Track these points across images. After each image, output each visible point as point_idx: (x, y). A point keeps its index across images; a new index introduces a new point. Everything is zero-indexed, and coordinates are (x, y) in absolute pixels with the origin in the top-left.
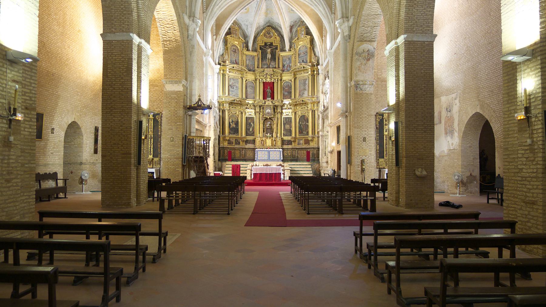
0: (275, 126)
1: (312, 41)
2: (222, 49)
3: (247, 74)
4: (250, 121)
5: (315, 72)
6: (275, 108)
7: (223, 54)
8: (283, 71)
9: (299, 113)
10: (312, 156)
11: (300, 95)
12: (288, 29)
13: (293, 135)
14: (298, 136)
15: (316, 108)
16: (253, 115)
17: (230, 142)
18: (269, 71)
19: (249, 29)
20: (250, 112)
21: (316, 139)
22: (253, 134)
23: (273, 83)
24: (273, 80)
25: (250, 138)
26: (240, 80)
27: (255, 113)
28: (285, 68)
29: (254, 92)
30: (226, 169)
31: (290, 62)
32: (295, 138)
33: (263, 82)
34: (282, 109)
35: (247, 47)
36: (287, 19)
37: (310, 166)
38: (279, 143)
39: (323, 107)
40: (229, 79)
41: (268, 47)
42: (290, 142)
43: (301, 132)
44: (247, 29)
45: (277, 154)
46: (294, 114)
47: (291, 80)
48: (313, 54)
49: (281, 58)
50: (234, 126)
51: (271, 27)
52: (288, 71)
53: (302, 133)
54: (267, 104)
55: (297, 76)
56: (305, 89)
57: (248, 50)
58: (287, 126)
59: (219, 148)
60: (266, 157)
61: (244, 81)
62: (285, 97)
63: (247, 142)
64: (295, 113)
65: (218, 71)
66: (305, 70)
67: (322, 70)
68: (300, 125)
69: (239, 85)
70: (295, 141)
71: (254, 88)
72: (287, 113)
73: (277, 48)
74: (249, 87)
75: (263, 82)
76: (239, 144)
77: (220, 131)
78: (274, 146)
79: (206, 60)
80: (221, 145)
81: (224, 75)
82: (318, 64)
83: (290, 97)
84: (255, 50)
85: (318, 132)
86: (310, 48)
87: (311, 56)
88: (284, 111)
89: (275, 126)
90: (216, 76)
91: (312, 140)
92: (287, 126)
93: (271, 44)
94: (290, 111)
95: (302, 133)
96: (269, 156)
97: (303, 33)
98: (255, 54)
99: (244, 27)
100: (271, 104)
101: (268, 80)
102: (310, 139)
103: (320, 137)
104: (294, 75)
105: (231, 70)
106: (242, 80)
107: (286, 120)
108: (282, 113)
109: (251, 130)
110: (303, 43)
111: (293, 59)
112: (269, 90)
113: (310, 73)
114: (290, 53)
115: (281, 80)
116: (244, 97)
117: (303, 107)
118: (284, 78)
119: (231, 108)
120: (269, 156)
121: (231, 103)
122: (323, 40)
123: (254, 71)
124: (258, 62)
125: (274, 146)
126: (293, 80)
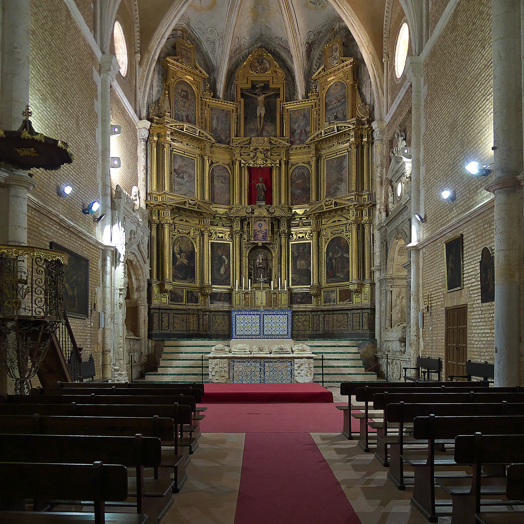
0: (275, 262)
1: (358, 65)
2: (155, 89)
3: (214, 149)
5: (365, 140)
6: (275, 222)
7: (158, 101)
8: (292, 143)
9: (328, 235)
10: (363, 328)
11: (329, 194)
12: (303, 49)
13: (314, 280)
14: (324, 283)
15: (366, 218)
16: (227, 240)
17: (175, 297)
18: (260, 143)
19: (218, 50)
20: (222, 234)
21: (367, 289)
22: (226, 281)
23: (270, 169)
24: (269, 161)
25: (218, 289)
26: (197, 162)
27: (231, 236)
28: (297, 137)
29: (230, 189)
30: (164, 356)
31: (308, 124)
32: (319, 287)
33: (249, 168)
34: (289, 227)
35: (213, 89)
36: (301, 23)
37: (355, 350)
38: (284, 299)
39: (384, 214)
40: (173, 158)
41: (258, 90)
42: (306, 298)
43: (331, 275)
44: (214, 51)
45: (279, 322)
46: (315, 234)
47: (309, 163)
48: (359, 100)
49: (286, 116)
50: (185, 261)
51: (266, 50)
52: (302, 142)
53: (334, 276)
54: (256, 214)
55: (323, 152)
56: (341, 180)
57: (215, 96)
58: (301, 263)
59: (149, 309)
60: (255, 330)
61: (207, 164)
62: (296, 200)
63: (214, 297)
64: (319, 235)
65: (145, 134)
66: (342, 135)
67: (382, 132)
68: (329, 260)
69: (197, 172)
70: (317, 296)
71: (229, 181)
72: (301, 233)
73: (278, 95)
74: (220, 177)
75: (249, 168)
76: (197, 302)
77: (151, 272)
78: (272, 304)
79: (104, 82)
80: (155, 302)
81: (160, 146)
82: (370, 120)
83: (307, 200)
84: (229, 97)
85: (372, 273)
86: (353, 86)
87: (354, 106)
88: (293, 230)
89: (275, 262)
90: (141, 147)
91: (358, 292)
92: (301, 263)
93: (266, 87)
94: (307, 229)
95: (334, 276)
97: (337, 54)
98: (230, 106)
99: (206, 47)
100: (265, 214)
101: (260, 162)
102: (352, 287)
103: (377, 285)
104: (317, 150)
105: (177, 133)
106: (203, 160)
107: (298, 250)
108: (289, 235)
109: (222, 271)
110: (336, 75)
111: (314, 115)
112: (261, 185)
113: (352, 139)
114: (307, 104)
115: (287, 163)
116: (207, 197)
117: (336, 219)
118: (294, 159)
119: (177, 221)
121: (178, 210)
122: (382, 64)
123: (229, 143)
124: (238, 123)
125: (272, 304)
126: (313, 163)
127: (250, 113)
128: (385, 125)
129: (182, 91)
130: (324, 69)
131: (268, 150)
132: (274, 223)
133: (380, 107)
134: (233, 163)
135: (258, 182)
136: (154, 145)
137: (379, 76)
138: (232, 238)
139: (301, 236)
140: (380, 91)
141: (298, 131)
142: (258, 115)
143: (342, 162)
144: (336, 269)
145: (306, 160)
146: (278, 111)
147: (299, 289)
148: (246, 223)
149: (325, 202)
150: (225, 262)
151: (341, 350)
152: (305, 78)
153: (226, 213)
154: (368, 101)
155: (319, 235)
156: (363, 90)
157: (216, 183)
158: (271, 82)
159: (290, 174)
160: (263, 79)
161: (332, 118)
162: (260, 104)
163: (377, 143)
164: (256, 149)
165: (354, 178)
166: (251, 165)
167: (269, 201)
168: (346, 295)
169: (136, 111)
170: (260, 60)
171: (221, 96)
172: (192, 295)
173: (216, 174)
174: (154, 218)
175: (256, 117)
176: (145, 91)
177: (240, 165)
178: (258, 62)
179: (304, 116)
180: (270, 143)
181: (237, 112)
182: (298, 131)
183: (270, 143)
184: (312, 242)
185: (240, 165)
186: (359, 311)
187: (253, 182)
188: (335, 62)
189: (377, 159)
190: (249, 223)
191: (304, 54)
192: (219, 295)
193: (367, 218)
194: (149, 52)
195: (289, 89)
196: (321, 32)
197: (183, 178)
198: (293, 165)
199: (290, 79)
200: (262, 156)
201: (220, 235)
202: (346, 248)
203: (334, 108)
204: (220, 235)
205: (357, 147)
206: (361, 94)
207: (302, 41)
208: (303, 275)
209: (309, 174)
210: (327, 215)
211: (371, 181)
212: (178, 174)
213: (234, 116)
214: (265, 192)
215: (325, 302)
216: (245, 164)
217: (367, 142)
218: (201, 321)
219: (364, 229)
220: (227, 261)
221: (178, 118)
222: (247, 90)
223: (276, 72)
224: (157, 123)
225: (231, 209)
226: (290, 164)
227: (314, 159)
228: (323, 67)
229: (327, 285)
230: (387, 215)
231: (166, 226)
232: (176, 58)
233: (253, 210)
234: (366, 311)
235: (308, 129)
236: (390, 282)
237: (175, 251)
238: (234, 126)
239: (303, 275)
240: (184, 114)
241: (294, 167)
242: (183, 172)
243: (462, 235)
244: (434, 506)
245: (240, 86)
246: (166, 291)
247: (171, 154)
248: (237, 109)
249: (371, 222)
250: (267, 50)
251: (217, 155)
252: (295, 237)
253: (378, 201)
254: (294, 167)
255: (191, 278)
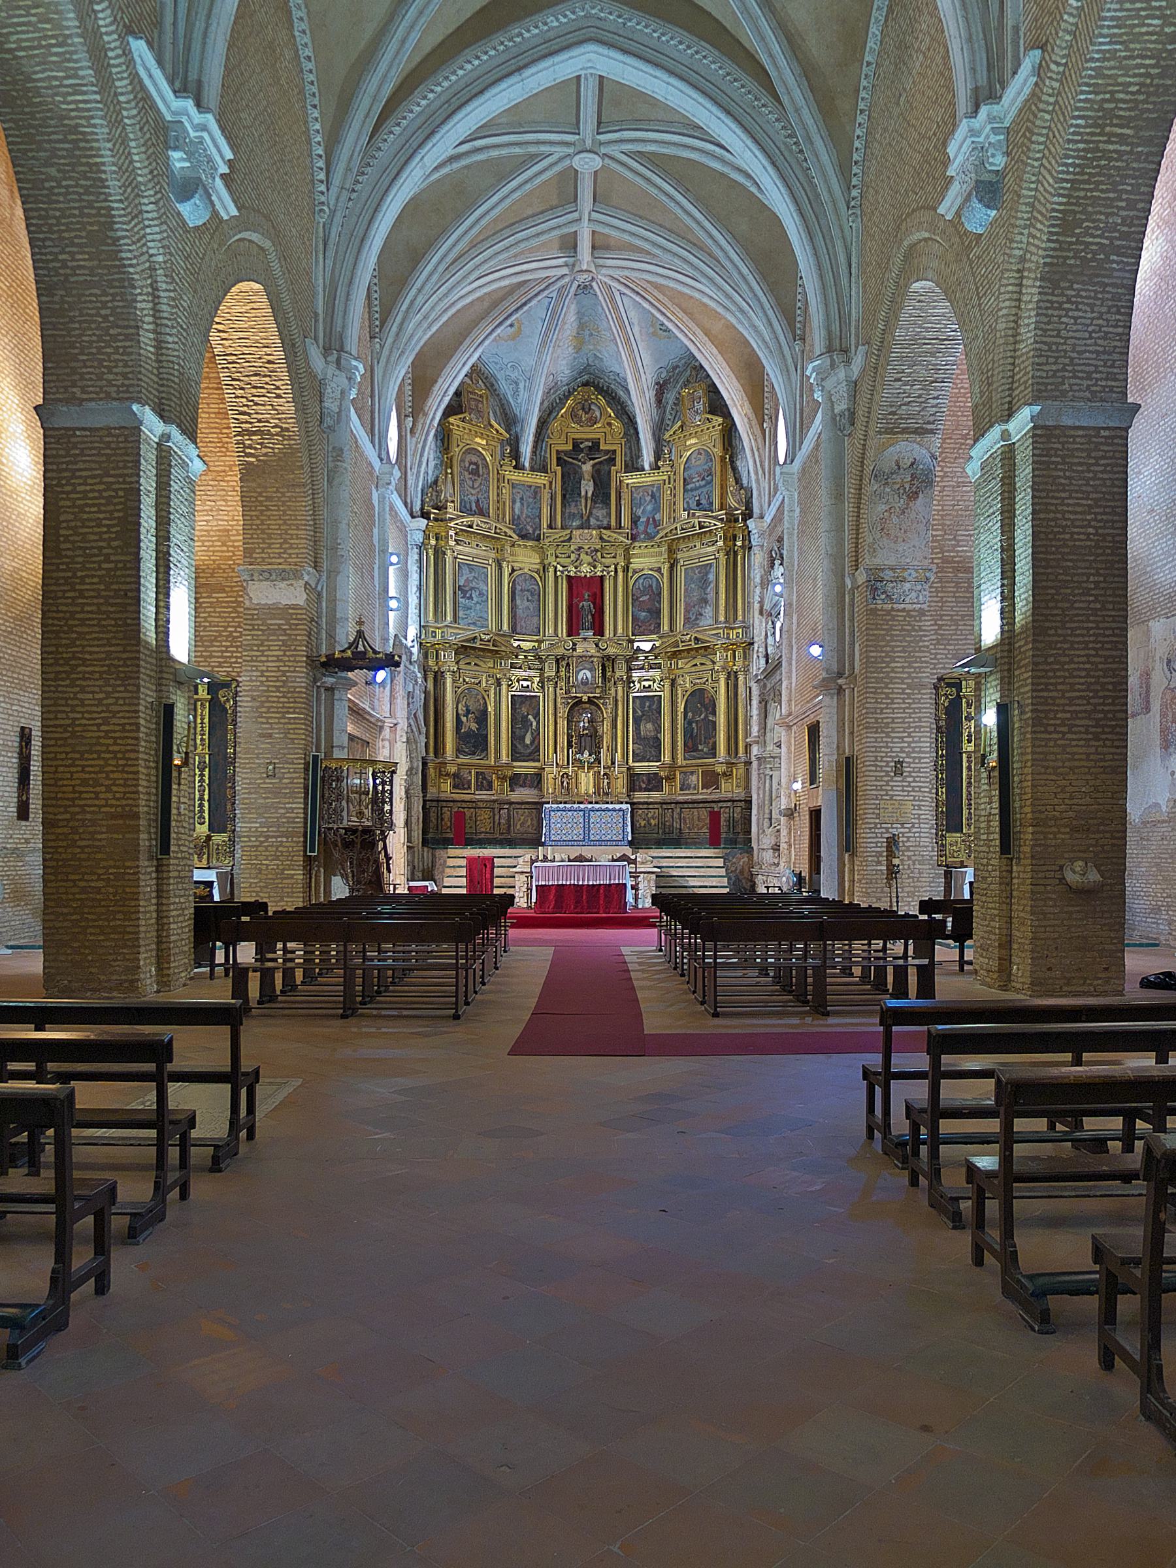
0: (607, 726)
1: (729, 433)
4: (524, 710)
6: (608, 663)
7: (436, 482)
8: (634, 538)
9: (686, 684)
10: (729, 829)
12: (650, 394)
13: (666, 757)
14: (680, 761)
15: (739, 663)
18: (587, 538)
19: (523, 395)
20: (524, 680)
22: (533, 754)
25: (525, 767)
26: (492, 570)
28: (641, 528)
29: (539, 610)
30: (448, 871)
31: (657, 509)
32: (673, 767)
34: (630, 669)
35: (516, 455)
39: (763, 661)
42: (654, 782)
43: (691, 747)
44: (516, 393)
46: (667, 684)
47: (659, 570)
48: (732, 480)
49: (625, 496)
50: (474, 726)
51: (595, 387)
52: (650, 537)
56: (706, 602)
57: (518, 467)
58: (647, 728)
59: (424, 801)
60: (577, 833)
63: (516, 781)
64: (673, 683)
65: (419, 537)
66: (704, 533)
68: (688, 723)
71: (538, 597)
73: (612, 461)
74: (527, 591)
75: (568, 577)
78: (602, 794)
80: (432, 791)
82: (748, 515)
84: (540, 467)
85: (748, 747)
86: (723, 459)
87: (723, 487)
88: (636, 675)
89: (607, 726)
90: (413, 556)
92: (647, 728)
96: (587, 829)
97: (700, 406)
98: (541, 479)
99: (505, 388)
100: (593, 651)
101: (585, 570)
102: (720, 769)
103: (755, 765)
104: (671, 551)
106: (500, 567)
107: (642, 706)
110: (698, 441)
112: (586, 604)
113: (721, 543)
115: (626, 569)
116: (505, 627)
118: (636, 563)
120: (587, 829)
121: (463, 650)
122: (763, 431)
123: (538, 539)
125: (602, 794)
126: (665, 571)
127: (570, 490)
128: (765, 525)
129: (471, 463)
130: (682, 426)
131: (597, 551)
132: (607, 664)
133: (760, 495)
134: (545, 569)
135: (583, 599)
136: (431, 552)
137: (758, 450)
138: (543, 687)
139: (647, 684)
140: (760, 472)
141: (643, 519)
142: (583, 493)
143: (707, 573)
144: (698, 737)
145: (656, 565)
146: (613, 485)
147: (641, 767)
148: (564, 663)
149: (685, 636)
150: (356, 368)
151: (699, 862)
152: (654, 434)
153: (534, 649)
154: (745, 482)
155: (673, 683)
156: (738, 463)
157: (518, 602)
158: (602, 441)
159: (631, 584)
160: (590, 436)
161: (693, 505)
162: (586, 476)
163: (755, 550)
164: (580, 548)
165: (722, 602)
166: (572, 574)
167: (600, 632)
168: (711, 780)
169: (406, 504)
170: (587, 406)
171: (527, 465)
172: (484, 778)
173: (519, 588)
174: (431, 663)
175: (580, 494)
176: (419, 472)
177: (555, 572)
178: (583, 409)
179: (653, 496)
180: (601, 538)
181: (550, 488)
182: (643, 519)
183: (601, 538)
184: (665, 695)
185: (555, 572)
186: (729, 804)
187: (575, 600)
188: (698, 418)
189: (757, 575)
190: (568, 665)
191: (653, 400)
192: (523, 777)
193: (740, 663)
194: (426, 415)
195: (630, 448)
196: (677, 366)
197: (471, 598)
198: (635, 572)
199: (632, 431)
200: (589, 559)
201: (525, 684)
202: (712, 708)
203: (697, 489)
204: (525, 684)
205: (727, 554)
206: (734, 469)
207: (650, 381)
208: (650, 747)
209: (659, 588)
210: (683, 655)
211: (747, 606)
212: (464, 592)
213: (546, 496)
214: (593, 616)
215: (681, 789)
216: (562, 572)
217: (743, 547)
218: (497, 817)
219: (737, 679)
220: (534, 724)
221: (465, 510)
222: (565, 453)
223: (610, 424)
224: (436, 520)
225: (540, 642)
226: (631, 571)
227: (667, 566)
228: (679, 423)
229: (684, 763)
230: (767, 662)
231: (448, 675)
232: (462, 416)
233: (574, 644)
234: (739, 804)
235: (657, 517)
236: (770, 763)
237: (460, 712)
238: (545, 511)
239: (650, 747)
240: (473, 498)
241: (637, 576)
242: (472, 589)
243: (818, 722)
244: (715, 977)
245: (555, 448)
246: (447, 774)
247: (454, 563)
248: (551, 483)
249: (746, 671)
250: (597, 387)
251: (520, 558)
252: (638, 685)
253: (756, 639)
254: (637, 576)
255: (482, 751)
